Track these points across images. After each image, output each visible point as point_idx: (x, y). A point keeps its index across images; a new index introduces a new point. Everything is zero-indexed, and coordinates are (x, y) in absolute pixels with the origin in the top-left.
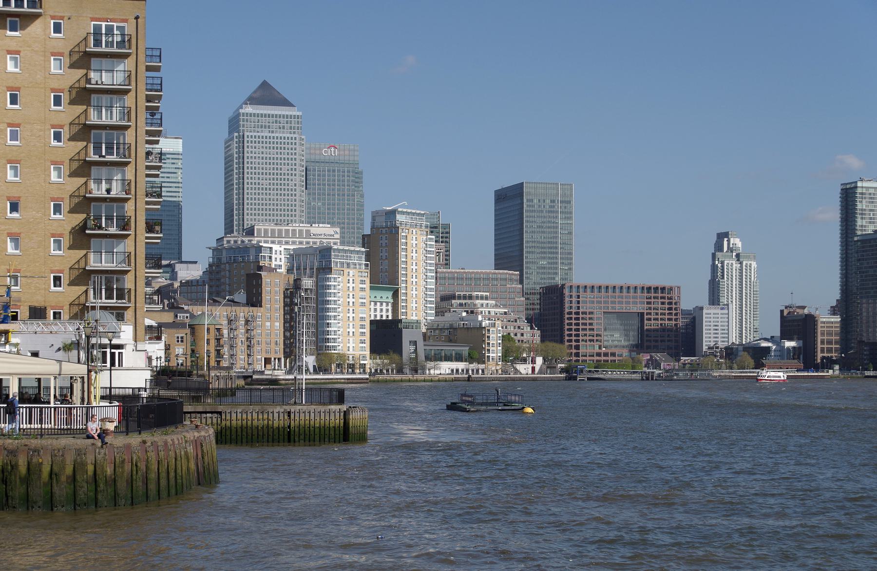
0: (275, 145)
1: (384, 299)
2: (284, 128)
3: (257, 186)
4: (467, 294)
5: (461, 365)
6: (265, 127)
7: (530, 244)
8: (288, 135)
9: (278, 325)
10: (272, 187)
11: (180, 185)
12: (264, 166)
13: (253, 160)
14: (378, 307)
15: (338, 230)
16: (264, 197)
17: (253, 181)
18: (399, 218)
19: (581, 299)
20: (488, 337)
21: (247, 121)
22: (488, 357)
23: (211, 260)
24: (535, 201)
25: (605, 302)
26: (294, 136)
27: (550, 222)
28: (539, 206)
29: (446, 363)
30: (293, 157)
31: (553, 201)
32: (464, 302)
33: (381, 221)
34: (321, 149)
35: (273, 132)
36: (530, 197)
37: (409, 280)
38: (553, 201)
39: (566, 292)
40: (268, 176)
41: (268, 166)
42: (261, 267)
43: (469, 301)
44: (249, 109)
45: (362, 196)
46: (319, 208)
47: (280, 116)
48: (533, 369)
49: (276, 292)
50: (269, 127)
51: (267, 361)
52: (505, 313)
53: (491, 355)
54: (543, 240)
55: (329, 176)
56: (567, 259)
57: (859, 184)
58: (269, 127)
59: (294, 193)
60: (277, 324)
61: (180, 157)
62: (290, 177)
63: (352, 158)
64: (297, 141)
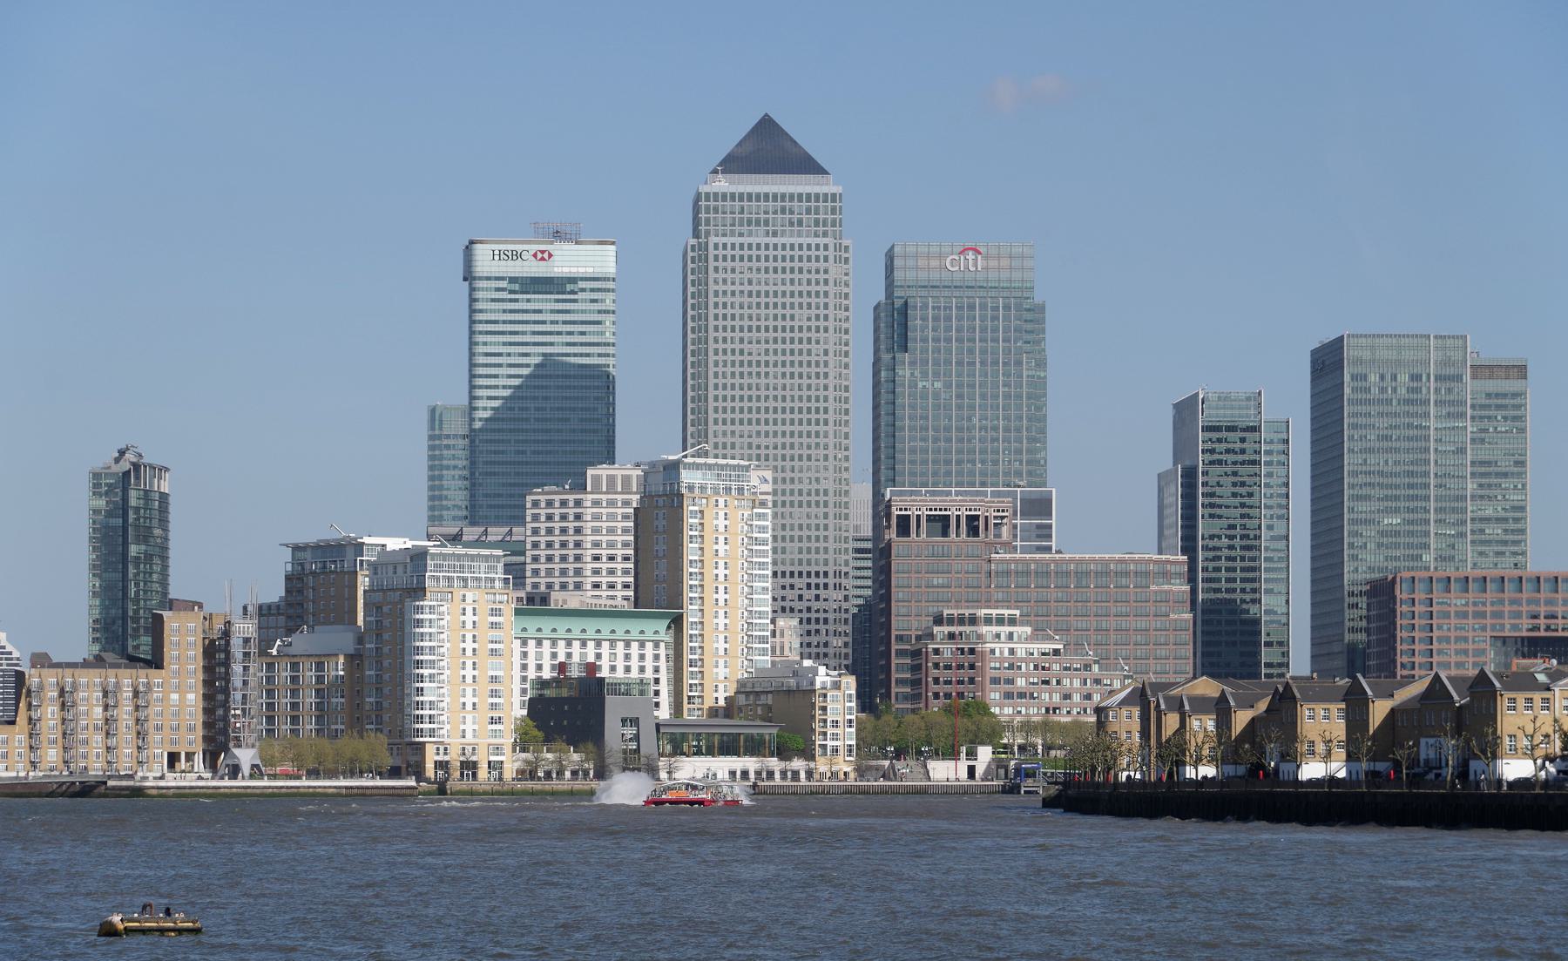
0: (780, 264)
2: (800, 223)
3: (738, 358)
4: (967, 612)
6: (758, 223)
7: (1361, 479)
10: (772, 358)
11: (610, 350)
12: (754, 311)
13: (729, 299)
16: (754, 381)
17: (729, 346)
18: (687, 477)
19: (1435, 608)
20: (824, 709)
21: (716, 210)
22: (824, 747)
23: (289, 567)
24: (1373, 378)
26: (822, 241)
27: (1410, 426)
28: (1383, 390)
29: (722, 758)
30: (821, 288)
31: (1416, 377)
32: (955, 629)
34: (941, 256)
35: (775, 234)
36: (1359, 370)
37: (709, 596)
38: (1416, 377)
39: (1401, 593)
40: (763, 334)
41: (763, 312)
42: (171, 601)
43: (967, 629)
44: (722, 184)
45: (1041, 364)
46: (936, 395)
47: (792, 197)
48: (971, 771)
49: (189, 644)
50: (767, 223)
51: (173, 758)
52: (1056, 652)
53: (830, 743)
55: (959, 318)
58: (767, 223)
59: (822, 370)
60: (191, 696)
61: (611, 285)
62: (814, 335)
63: (1017, 275)
64: (831, 253)
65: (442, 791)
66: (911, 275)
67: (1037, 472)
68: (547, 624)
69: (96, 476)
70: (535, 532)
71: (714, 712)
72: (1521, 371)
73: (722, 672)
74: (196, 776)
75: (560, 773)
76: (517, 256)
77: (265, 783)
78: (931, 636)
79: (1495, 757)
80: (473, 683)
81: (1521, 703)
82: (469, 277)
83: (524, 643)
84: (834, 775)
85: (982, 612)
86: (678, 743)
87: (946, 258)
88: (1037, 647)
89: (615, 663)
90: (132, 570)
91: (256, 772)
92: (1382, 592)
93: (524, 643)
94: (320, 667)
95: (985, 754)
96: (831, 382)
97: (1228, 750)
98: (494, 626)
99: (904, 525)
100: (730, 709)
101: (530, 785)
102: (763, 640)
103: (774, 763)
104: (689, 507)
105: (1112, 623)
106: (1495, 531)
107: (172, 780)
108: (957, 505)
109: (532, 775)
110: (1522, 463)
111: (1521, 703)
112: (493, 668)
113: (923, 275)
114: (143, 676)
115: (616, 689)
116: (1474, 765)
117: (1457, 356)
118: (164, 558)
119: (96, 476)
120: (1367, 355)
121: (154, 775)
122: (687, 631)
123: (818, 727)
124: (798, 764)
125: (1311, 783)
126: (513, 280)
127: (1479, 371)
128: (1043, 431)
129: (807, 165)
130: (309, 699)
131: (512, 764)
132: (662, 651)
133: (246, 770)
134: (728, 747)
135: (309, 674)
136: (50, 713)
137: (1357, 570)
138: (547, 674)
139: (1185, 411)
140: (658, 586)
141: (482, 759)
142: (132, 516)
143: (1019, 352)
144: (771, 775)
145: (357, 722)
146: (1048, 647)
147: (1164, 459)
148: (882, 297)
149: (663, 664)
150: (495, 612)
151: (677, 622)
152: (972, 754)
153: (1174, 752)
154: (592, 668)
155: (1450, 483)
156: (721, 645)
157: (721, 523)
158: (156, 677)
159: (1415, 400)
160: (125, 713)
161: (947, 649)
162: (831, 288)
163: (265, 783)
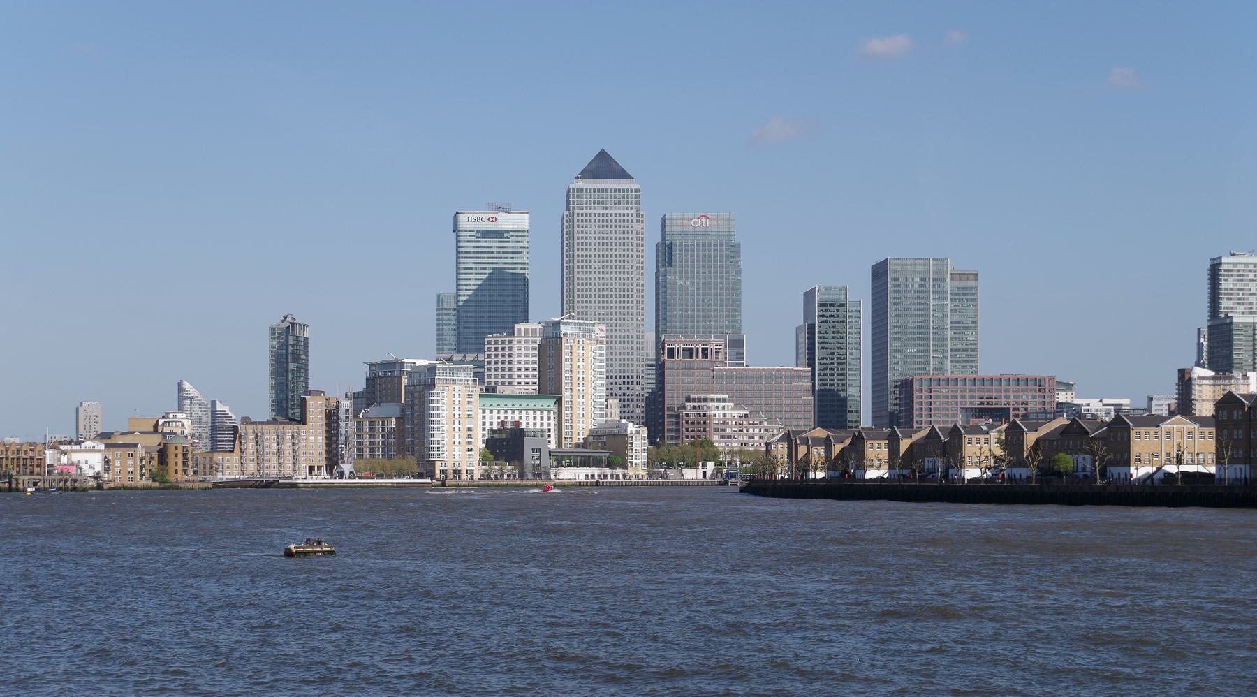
1: (545, 407)
5: (596, 471)
7: (896, 330)
8: (626, 212)
9: (321, 439)
14: (538, 414)
18: (563, 329)
24: (902, 280)
25: (963, 397)
26: (630, 212)
31: (923, 279)
33: (549, 333)
34: (689, 220)
36: (895, 276)
37: (575, 388)
38: (924, 279)
39: (916, 386)
43: (702, 404)
44: (581, 184)
45: (738, 273)
51: (311, 469)
54: (911, 324)
56: (942, 345)
57: (1224, 260)
63: (726, 229)
65: (444, 485)
66: (674, 229)
68: (495, 402)
69: (273, 329)
70: (489, 356)
71: (577, 445)
72: (975, 276)
73: (581, 425)
74: (322, 478)
75: (502, 476)
76: (480, 219)
77: (356, 481)
78: (684, 408)
80: (459, 432)
81: (974, 440)
82: (456, 230)
83: (484, 411)
87: (691, 219)
88: (736, 413)
89: (529, 421)
90: (290, 376)
91: (352, 475)
92: (906, 386)
93: (484, 411)
94: (383, 424)
95: (711, 466)
97: (830, 464)
98: (469, 403)
100: (585, 444)
101: (487, 482)
102: (601, 409)
103: (607, 471)
104: (565, 344)
106: (962, 356)
107: (311, 480)
108: (697, 343)
109: (488, 477)
110: (975, 322)
111: (974, 440)
113: (680, 229)
114: (296, 428)
119: (273, 329)
120: (899, 268)
121: (302, 477)
123: (628, 452)
124: (619, 471)
125: (815, 480)
126: (478, 232)
128: (739, 306)
129: (624, 175)
130: (378, 439)
131: (478, 471)
132: (552, 415)
133: (347, 475)
134: (585, 463)
136: (250, 447)
137: (894, 375)
138: (495, 427)
139: (809, 296)
140: (550, 383)
141: (463, 468)
144: (605, 476)
147: (799, 320)
149: (552, 421)
150: (470, 396)
151: (559, 401)
152: (704, 466)
153: (804, 465)
154: (517, 424)
156: (581, 412)
157: (581, 352)
158: (302, 428)
159: (923, 291)
160: (287, 446)
161: (693, 414)
162: (634, 235)
163: (356, 481)
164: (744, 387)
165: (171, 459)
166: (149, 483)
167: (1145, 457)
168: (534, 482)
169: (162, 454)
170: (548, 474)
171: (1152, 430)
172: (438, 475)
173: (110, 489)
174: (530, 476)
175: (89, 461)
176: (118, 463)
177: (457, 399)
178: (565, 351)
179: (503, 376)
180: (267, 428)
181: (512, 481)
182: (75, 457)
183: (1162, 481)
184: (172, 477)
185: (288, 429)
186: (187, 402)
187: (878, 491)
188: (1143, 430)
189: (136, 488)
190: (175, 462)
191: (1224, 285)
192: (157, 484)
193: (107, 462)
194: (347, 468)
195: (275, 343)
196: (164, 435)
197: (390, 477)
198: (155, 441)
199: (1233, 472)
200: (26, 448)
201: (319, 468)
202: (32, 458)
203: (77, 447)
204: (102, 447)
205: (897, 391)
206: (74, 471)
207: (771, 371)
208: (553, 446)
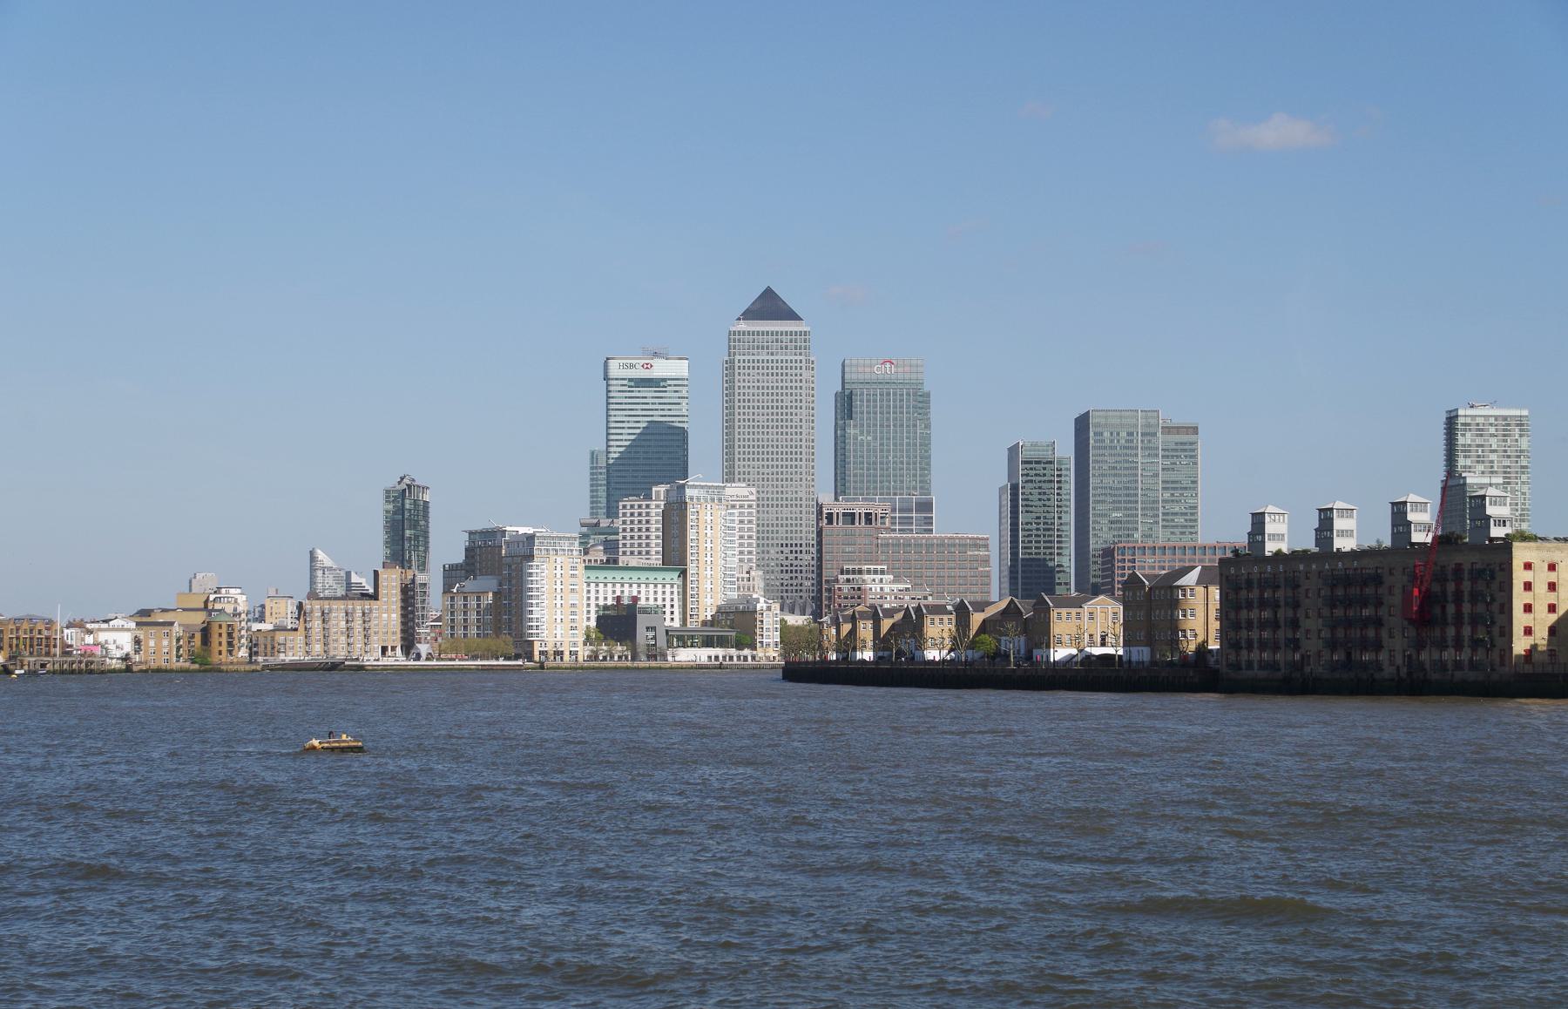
5: (720, 652)
9: (396, 617)
15: (754, 490)
18: (689, 492)
24: (1107, 434)
37: (702, 558)
44: (743, 326)
45: (928, 426)
51: (384, 649)
54: (1116, 485)
57: (1461, 412)
63: (914, 376)
65: (542, 667)
66: (854, 376)
67: (926, 490)
68: (618, 575)
69: (387, 491)
70: (624, 522)
71: (705, 623)
72: (1195, 430)
73: (709, 601)
74: (398, 659)
75: (612, 657)
76: (632, 366)
77: (434, 663)
78: (837, 581)
79: (1048, 647)
80: (562, 609)
81: (937, 621)
82: (606, 378)
84: (768, 658)
85: (865, 567)
86: (683, 639)
87: (875, 366)
88: (895, 587)
89: (647, 597)
90: (407, 545)
92: (1108, 553)
94: (479, 599)
96: (804, 437)
97: (880, 643)
98: (573, 576)
99: (830, 517)
100: (713, 622)
101: (592, 664)
102: (732, 583)
103: (733, 652)
104: (690, 510)
105: (946, 573)
106: (1180, 520)
108: (860, 508)
109: (596, 658)
110: (1195, 482)
111: (937, 621)
112: (573, 598)
113: (861, 376)
114: (367, 604)
115: (645, 611)
116: (1036, 652)
117: (1153, 421)
118: (426, 538)
119: (387, 491)
120: (1103, 421)
121: (372, 659)
122: (689, 578)
123: (758, 631)
124: (746, 652)
125: (933, 662)
127: (1168, 430)
128: (929, 464)
129: (792, 316)
130: (473, 617)
131: (583, 652)
132: (675, 589)
133: (424, 656)
134: (708, 642)
135: (473, 603)
136: (316, 624)
137: (1095, 544)
138: (610, 602)
139: (1013, 451)
140: (675, 557)
141: (566, 649)
142: (407, 515)
143: (915, 419)
144: (731, 658)
145: (498, 632)
146: (901, 586)
147: (1004, 481)
148: (839, 389)
149: (675, 596)
150: (574, 568)
151: (684, 573)
153: (848, 644)
154: (635, 599)
155: (1150, 494)
156: (709, 586)
157: (709, 518)
158: (375, 605)
159: (1130, 446)
160: (357, 625)
161: (846, 588)
162: (804, 384)
163: (434, 663)
164: (913, 556)
165: (215, 639)
166: (187, 665)
167: (1066, 639)
168: (647, 664)
169: (206, 632)
170: (664, 656)
171: (1074, 611)
172: (537, 658)
173: (141, 671)
174: (643, 658)
175: (118, 641)
176: (152, 643)
177: (559, 571)
178: (690, 517)
179: (640, 545)
180: (335, 605)
181: (624, 664)
182: (102, 637)
183: (1082, 663)
184: (215, 659)
185: (358, 607)
186: (319, 573)
187: (1091, 675)
188: (1064, 611)
189: (171, 671)
190: (219, 641)
191: (1461, 440)
192: (196, 666)
193: (137, 641)
194: (423, 648)
195: (390, 507)
196: (210, 612)
197: (475, 658)
198: (198, 619)
199: (1142, 654)
200: (40, 626)
201: (393, 648)
202: (47, 638)
203: (105, 626)
204: (133, 625)
205: (1100, 560)
206: (98, 651)
207: (943, 539)
208: (677, 624)
